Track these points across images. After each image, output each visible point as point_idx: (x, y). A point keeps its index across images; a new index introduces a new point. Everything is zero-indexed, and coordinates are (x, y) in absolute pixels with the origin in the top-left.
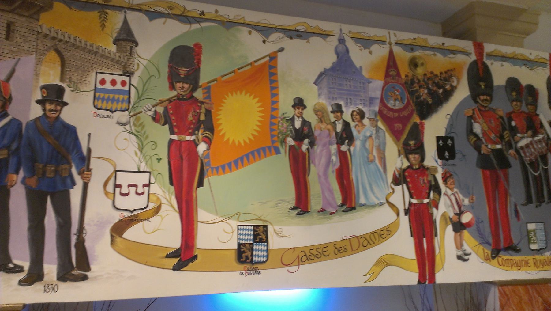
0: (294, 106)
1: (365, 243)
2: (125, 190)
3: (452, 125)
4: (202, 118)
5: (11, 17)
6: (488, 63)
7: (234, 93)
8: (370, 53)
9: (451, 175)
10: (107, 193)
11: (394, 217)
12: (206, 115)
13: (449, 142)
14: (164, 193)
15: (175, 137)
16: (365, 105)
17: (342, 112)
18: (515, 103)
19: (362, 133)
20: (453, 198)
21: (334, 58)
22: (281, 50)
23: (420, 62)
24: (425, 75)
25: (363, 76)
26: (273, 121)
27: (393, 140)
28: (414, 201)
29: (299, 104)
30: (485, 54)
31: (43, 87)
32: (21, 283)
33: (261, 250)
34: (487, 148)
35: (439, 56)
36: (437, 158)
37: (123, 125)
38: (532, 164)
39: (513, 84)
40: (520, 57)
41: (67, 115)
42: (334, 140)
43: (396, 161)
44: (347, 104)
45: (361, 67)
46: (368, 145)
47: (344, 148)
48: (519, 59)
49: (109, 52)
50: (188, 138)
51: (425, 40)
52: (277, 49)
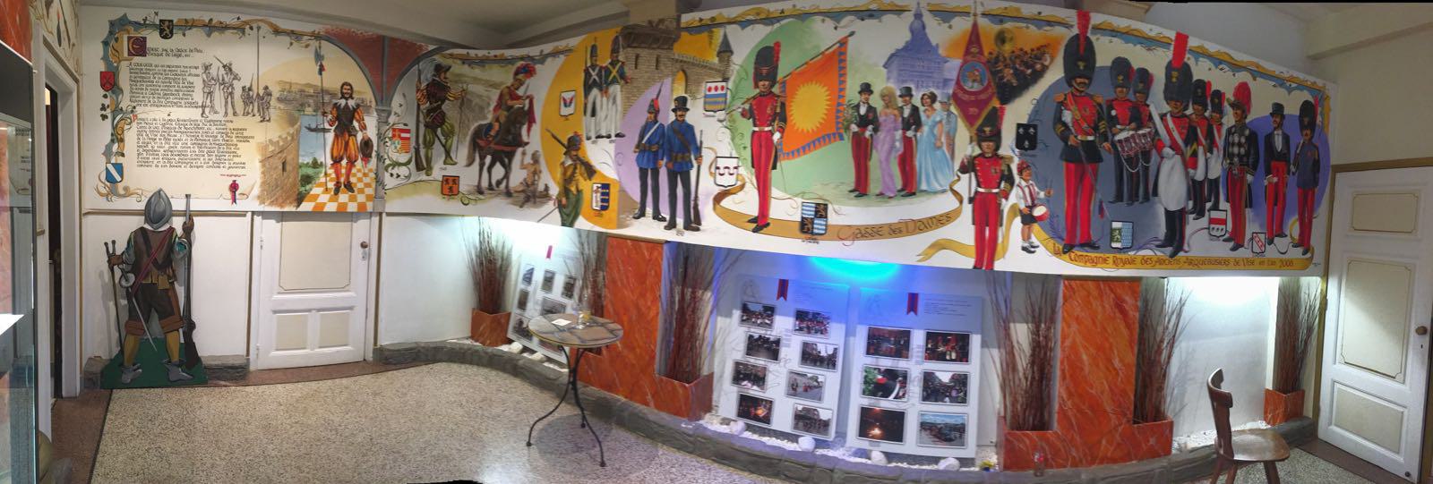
0: (860, 93)
1: (922, 227)
2: (722, 171)
3: (1037, 111)
4: (778, 110)
5: (658, 52)
6: (1093, 38)
7: (818, 125)
8: (950, 27)
9: (1028, 166)
10: (711, 173)
11: (957, 204)
12: (781, 108)
13: (1032, 130)
14: (748, 174)
15: (756, 129)
16: (938, 88)
17: (911, 96)
18: (1120, 89)
19: (932, 118)
20: (1027, 190)
21: (907, 36)
22: (852, 34)
23: (1008, 36)
24: (1013, 52)
25: (939, 55)
26: (839, 108)
27: (966, 126)
28: (981, 190)
29: (866, 89)
30: (1090, 26)
31: (676, 100)
32: (666, 228)
33: (821, 225)
34: (1077, 139)
35: (1032, 27)
36: (1014, 147)
37: (721, 121)
38: (1129, 160)
39: (1121, 65)
40: (1135, 33)
41: (690, 118)
42: (900, 126)
43: (966, 147)
44: (917, 87)
45: (937, 45)
46: (936, 131)
47: (910, 134)
48: (1133, 35)
49: (714, 64)
50: (767, 129)
51: (1018, 10)
52: (847, 34)
